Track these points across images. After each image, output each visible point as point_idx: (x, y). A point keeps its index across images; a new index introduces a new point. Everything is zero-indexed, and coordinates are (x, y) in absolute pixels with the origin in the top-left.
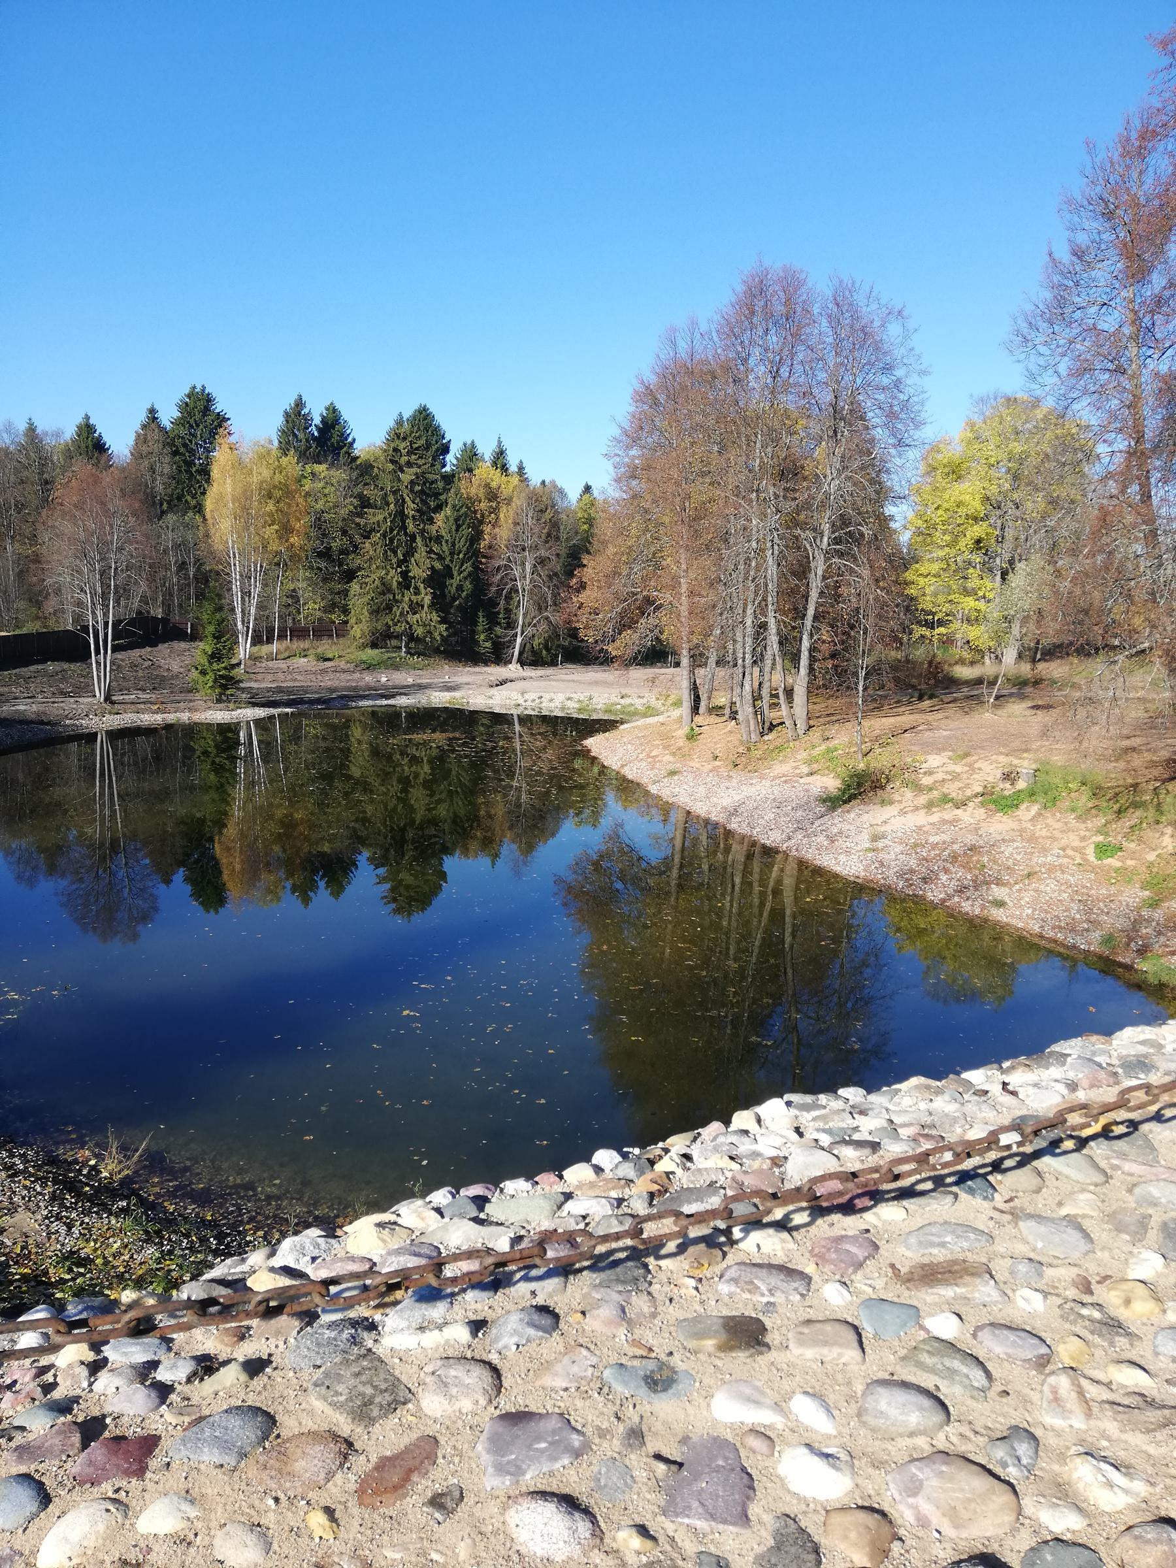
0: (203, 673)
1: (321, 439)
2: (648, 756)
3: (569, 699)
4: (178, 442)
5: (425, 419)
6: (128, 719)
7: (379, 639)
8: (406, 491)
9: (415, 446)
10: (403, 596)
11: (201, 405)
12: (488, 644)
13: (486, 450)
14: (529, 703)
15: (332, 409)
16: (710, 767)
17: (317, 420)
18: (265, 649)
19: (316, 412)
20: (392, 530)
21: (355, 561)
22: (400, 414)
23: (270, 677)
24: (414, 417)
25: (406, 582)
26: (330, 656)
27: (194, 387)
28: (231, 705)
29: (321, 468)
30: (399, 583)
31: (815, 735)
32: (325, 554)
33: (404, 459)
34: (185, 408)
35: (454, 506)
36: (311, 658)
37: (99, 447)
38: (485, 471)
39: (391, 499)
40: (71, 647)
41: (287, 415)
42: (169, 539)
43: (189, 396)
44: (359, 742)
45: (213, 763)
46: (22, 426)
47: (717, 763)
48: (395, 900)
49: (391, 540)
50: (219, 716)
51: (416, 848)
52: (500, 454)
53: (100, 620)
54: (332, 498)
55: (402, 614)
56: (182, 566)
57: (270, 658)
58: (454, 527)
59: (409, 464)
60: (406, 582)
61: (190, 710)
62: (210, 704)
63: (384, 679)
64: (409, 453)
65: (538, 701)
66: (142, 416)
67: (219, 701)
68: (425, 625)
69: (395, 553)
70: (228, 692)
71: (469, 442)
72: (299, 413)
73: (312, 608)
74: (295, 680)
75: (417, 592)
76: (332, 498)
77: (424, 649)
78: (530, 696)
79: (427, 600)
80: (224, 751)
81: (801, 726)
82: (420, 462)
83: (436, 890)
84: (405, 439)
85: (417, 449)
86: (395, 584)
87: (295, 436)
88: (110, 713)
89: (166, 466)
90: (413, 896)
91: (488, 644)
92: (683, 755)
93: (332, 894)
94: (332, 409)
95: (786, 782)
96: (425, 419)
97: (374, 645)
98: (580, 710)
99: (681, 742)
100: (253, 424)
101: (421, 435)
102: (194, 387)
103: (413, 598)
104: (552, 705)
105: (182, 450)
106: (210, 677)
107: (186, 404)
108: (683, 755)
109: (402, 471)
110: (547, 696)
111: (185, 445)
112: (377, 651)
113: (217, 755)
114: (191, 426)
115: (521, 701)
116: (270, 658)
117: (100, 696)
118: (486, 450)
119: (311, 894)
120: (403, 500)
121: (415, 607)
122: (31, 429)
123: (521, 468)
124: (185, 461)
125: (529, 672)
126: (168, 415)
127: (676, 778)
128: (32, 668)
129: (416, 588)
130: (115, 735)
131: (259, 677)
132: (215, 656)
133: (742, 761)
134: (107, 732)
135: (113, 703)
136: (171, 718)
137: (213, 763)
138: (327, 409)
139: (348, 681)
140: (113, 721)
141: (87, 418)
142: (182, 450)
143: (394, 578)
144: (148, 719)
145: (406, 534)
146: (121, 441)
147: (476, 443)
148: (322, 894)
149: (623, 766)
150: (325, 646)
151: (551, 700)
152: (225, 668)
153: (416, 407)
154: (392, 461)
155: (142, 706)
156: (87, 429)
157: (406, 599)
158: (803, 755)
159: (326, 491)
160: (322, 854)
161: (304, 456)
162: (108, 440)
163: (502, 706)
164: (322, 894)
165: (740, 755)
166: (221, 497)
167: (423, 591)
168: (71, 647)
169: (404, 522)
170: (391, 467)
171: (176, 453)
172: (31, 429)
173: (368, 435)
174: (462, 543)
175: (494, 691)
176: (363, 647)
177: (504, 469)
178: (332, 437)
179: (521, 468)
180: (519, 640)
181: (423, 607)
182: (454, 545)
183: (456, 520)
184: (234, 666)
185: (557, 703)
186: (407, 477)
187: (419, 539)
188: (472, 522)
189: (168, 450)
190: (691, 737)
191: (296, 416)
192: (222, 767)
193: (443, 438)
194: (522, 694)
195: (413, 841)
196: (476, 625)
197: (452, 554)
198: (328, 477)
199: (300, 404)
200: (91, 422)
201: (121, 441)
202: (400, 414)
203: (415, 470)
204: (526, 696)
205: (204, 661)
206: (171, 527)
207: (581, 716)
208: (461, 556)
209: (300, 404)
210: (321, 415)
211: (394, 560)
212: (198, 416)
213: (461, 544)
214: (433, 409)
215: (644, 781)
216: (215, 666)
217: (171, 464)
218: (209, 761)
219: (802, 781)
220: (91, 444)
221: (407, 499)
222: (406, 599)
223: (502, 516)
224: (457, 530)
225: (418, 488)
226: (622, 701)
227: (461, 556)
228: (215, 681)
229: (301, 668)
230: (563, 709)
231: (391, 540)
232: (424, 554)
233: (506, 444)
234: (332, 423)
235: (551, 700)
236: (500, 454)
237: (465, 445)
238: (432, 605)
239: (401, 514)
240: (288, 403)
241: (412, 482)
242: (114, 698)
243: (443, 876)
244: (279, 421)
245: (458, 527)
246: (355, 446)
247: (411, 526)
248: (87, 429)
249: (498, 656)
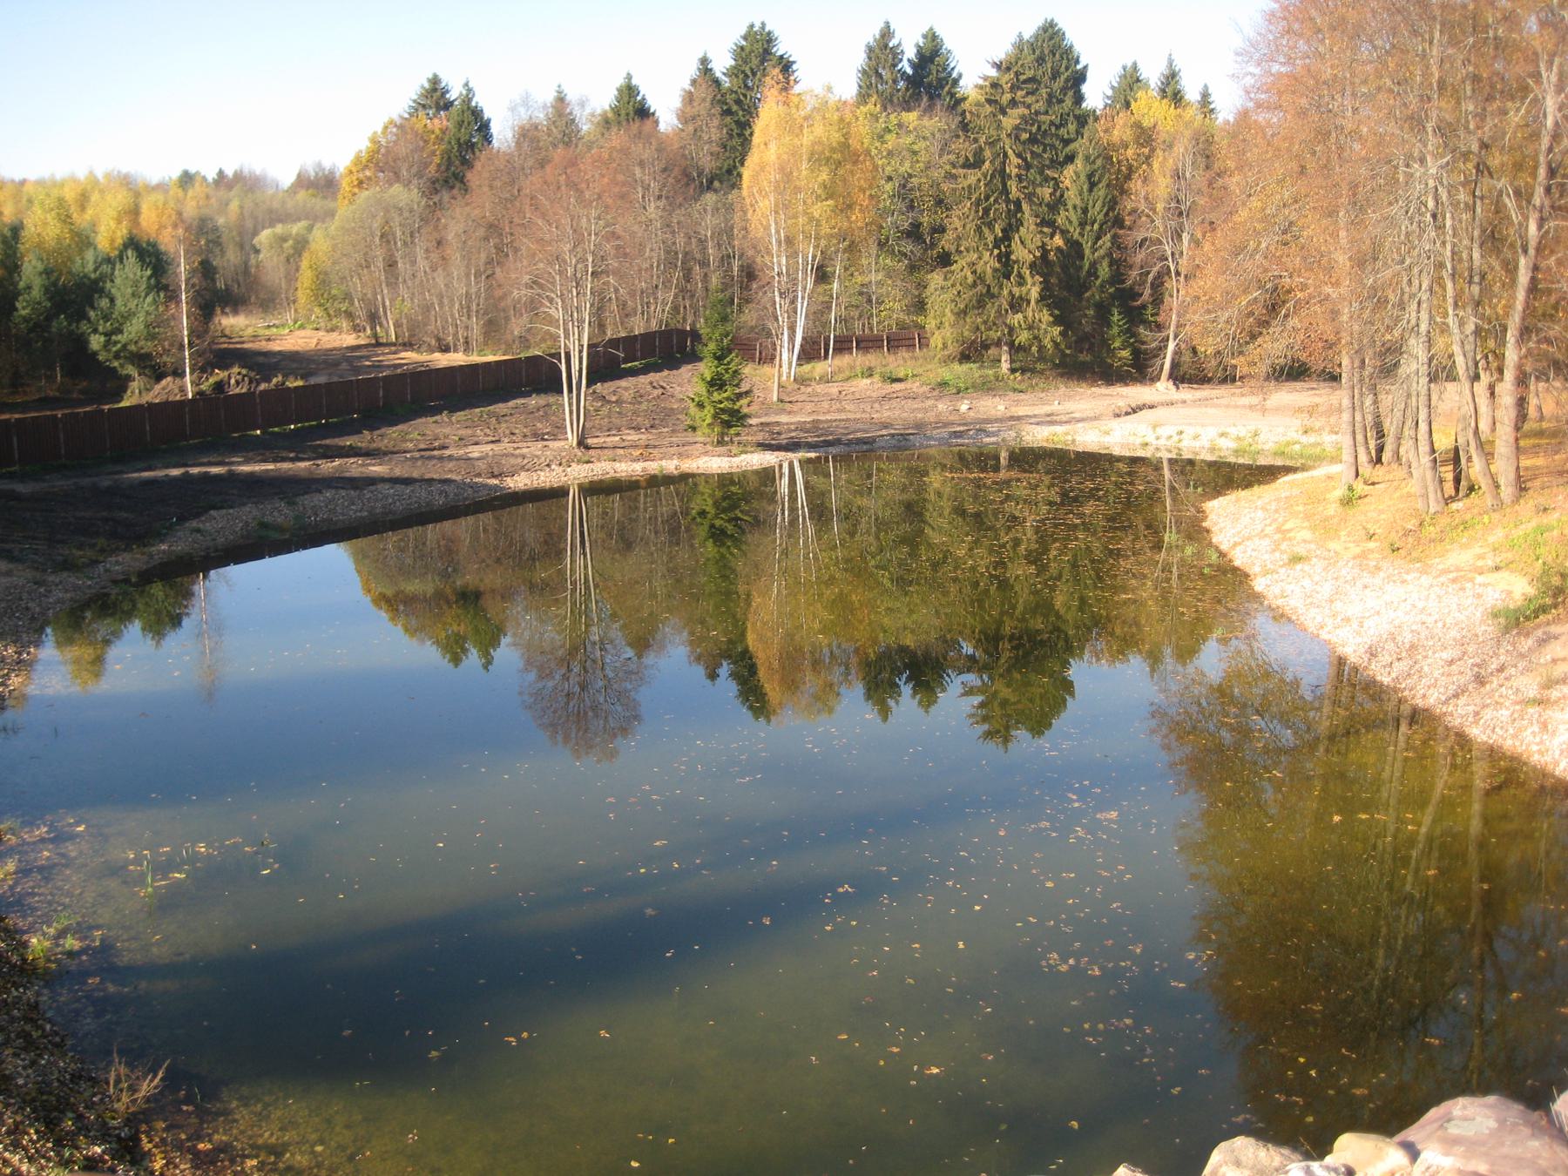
0: (701, 406)
1: (922, 79)
2: (1278, 530)
3: (1222, 435)
4: (730, 98)
5: (1051, 38)
6: (603, 469)
7: (971, 352)
8: (1007, 141)
9: (1022, 78)
10: (1001, 287)
11: (759, 48)
12: (1125, 353)
13: (1152, 74)
14: (1162, 442)
15: (932, 37)
16: (1358, 550)
17: (910, 53)
18: (820, 368)
19: (909, 45)
20: (987, 198)
21: (946, 242)
22: (1020, 35)
23: (809, 407)
24: (1036, 37)
25: (1006, 264)
26: (901, 375)
27: (752, 26)
28: (735, 449)
29: (911, 117)
30: (995, 270)
31: (1528, 504)
32: (914, 233)
33: (1007, 97)
34: (741, 53)
35: (1087, 158)
36: (876, 378)
37: (643, 112)
38: (1148, 107)
39: (988, 153)
40: (535, 376)
41: (870, 50)
42: (709, 225)
43: (745, 38)
44: (939, 494)
45: (712, 526)
46: (549, 97)
47: (1372, 545)
48: (985, 719)
49: (986, 211)
50: (714, 463)
51: (1016, 648)
52: (1172, 76)
53: (576, 349)
54: (923, 157)
55: (999, 312)
56: (726, 259)
57: (825, 379)
58: (1086, 187)
59: (1013, 103)
60: (1006, 264)
61: (680, 455)
62: (709, 447)
63: (964, 407)
64: (1013, 88)
65: (1176, 438)
66: (692, 69)
67: (720, 443)
68: (1030, 328)
69: (992, 229)
70: (732, 431)
71: (1129, 65)
72: (886, 46)
73: (893, 311)
74: (843, 410)
75: (1021, 281)
76: (923, 157)
77: (1034, 365)
78: (1164, 431)
79: (1034, 293)
80: (724, 511)
81: (1507, 491)
82: (1029, 100)
83: (1058, 705)
84: (1008, 69)
85: (1025, 82)
86: (989, 271)
87: (880, 76)
88: (579, 462)
89: (714, 131)
90: (1000, 722)
91: (1125, 353)
92: (1326, 529)
93: (920, 702)
94: (932, 37)
95: (1454, 581)
96: (1051, 38)
97: (964, 358)
98: (1236, 452)
99: (1333, 509)
100: (828, 69)
101: (1047, 65)
102: (752, 26)
103: (1016, 291)
104: (1197, 444)
105: (735, 108)
106: (709, 411)
107: (742, 48)
108: (1326, 529)
109: (1004, 113)
110: (1189, 432)
111: (738, 102)
112: (966, 367)
113: (716, 516)
114: (747, 76)
115: (1151, 438)
116: (825, 379)
117: (572, 439)
118: (1152, 74)
119: (891, 703)
120: (1006, 155)
121: (1017, 304)
122: (561, 100)
123: (1205, 95)
124: (738, 123)
125: (1187, 393)
126: (722, 63)
127: (1299, 567)
128: (511, 404)
129: (1020, 275)
130: (594, 489)
131: (795, 407)
132: (716, 383)
133: (1407, 545)
134: (580, 486)
135: (588, 448)
136: (653, 467)
137: (712, 526)
138: (925, 37)
139: (913, 411)
140: (577, 474)
141: (629, 77)
142: (735, 108)
143: (988, 263)
144: (628, 468)
145: (1008, 201)
146: (666, 108)
147: (1139, 66)
148: (906, 701)
149: (1236, 544)
150: (898, 363)
151: (1196, 437)
152: (728, 399)
153: (1040, 22)
154: (989, 101)
155: (621, 452)
156: (629, 91)
157: (1005, 292)
158: (1497, 536)
159: (916, 147)
160: (903, 650)
161: (887, 102)
162: (653, 104)
163: (1122, 446)
164: (906, 701)
165: (1407, 533)
166: (763, 167)
167: (1029, 280)
168: (535, 376)
169: (1004, 185)
170: (989, 109)
171: (728, 112)
172: (561, 100)
173: (973, 67)
174: (1098, 207)
175: (1116, 424)
176: (947, 360)
177: (1177, 98)
178: (930, 73)
179: (1205, 95)
180: (1171, 346)
181: (1029, 302)
182: (1085, 211)
183: (1090, 176)
184: (739, 396)
185: (1204, 442)
186: (1010, 121)
187: (1025, 206)
188: (1113, 177)
189: (717, 110)
190: (1347, 502)
191: (882, 51)
192: (723, 532)
193: (1077, 62)
194: (1154, 427)
195: (1012, 638)
196: (1109, 326)
197: (1082, 224)
198: (922, 125)
199: (886, 33)
200: (634, 82)
201: (666, 108)
202: (1020, 35)
203: (1022, 110)
204: (1160, 431)
205: (701, 389)
206: (706, 212)
207: (1241, 461)
208: (1096, 226)
209: (886, 33)
210: (918, 46)
211: (990, 239)
212: (755, 62)
213: (1097, 212)
214: (1062, 24)
215: (1254, 570)
216: (716, 396)
217: (720, 128)
218: (706, 523)
219: (1479, 579)
220: (633, 109)
221: (1010, 152)
222: (1005, 292)
223: (1156, 165)
224: (1091, 190)
225: (1025, 136)
226: (1305, 439)
227: (1096, 226)
228: (715, 416)
229: (856, 394)
230: (1212, 450)
231: (986, 211)
232: (1032, 227)
233: (1179, 65)
234: (931, 55)
235: (1196, 437)
236: (1172, 76)
237: (1124, 68)
238: (1042, 298)
239: (1003, 174)
240: (871, 34)
241: (1017, 128)
242: (590, 441)
243: (1068, 686)
244: (859, 59)
245: (1092, 185)
246: (961, 83)
247: (1014, 189)
248: (629, 91)
249: (1140, 369)
